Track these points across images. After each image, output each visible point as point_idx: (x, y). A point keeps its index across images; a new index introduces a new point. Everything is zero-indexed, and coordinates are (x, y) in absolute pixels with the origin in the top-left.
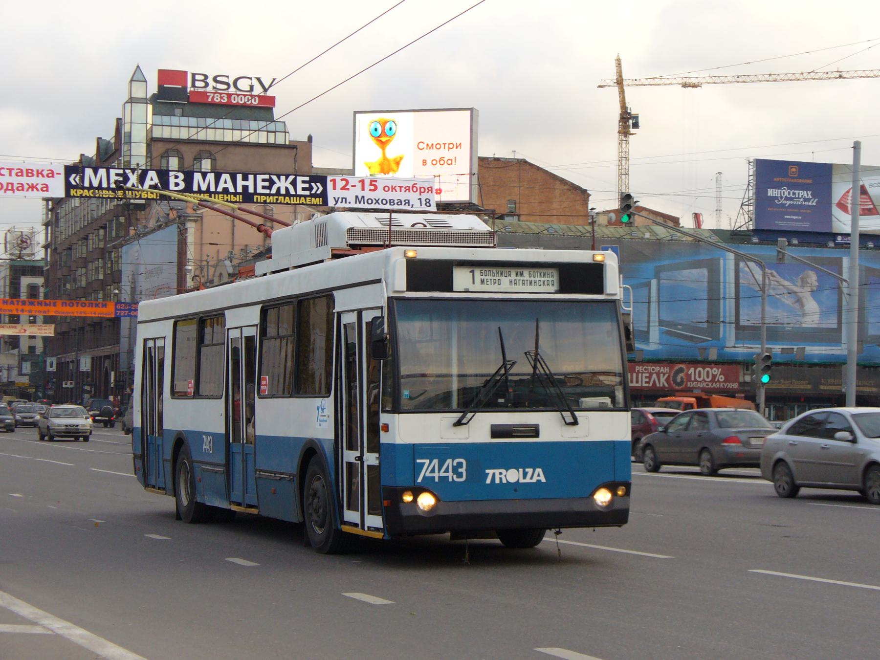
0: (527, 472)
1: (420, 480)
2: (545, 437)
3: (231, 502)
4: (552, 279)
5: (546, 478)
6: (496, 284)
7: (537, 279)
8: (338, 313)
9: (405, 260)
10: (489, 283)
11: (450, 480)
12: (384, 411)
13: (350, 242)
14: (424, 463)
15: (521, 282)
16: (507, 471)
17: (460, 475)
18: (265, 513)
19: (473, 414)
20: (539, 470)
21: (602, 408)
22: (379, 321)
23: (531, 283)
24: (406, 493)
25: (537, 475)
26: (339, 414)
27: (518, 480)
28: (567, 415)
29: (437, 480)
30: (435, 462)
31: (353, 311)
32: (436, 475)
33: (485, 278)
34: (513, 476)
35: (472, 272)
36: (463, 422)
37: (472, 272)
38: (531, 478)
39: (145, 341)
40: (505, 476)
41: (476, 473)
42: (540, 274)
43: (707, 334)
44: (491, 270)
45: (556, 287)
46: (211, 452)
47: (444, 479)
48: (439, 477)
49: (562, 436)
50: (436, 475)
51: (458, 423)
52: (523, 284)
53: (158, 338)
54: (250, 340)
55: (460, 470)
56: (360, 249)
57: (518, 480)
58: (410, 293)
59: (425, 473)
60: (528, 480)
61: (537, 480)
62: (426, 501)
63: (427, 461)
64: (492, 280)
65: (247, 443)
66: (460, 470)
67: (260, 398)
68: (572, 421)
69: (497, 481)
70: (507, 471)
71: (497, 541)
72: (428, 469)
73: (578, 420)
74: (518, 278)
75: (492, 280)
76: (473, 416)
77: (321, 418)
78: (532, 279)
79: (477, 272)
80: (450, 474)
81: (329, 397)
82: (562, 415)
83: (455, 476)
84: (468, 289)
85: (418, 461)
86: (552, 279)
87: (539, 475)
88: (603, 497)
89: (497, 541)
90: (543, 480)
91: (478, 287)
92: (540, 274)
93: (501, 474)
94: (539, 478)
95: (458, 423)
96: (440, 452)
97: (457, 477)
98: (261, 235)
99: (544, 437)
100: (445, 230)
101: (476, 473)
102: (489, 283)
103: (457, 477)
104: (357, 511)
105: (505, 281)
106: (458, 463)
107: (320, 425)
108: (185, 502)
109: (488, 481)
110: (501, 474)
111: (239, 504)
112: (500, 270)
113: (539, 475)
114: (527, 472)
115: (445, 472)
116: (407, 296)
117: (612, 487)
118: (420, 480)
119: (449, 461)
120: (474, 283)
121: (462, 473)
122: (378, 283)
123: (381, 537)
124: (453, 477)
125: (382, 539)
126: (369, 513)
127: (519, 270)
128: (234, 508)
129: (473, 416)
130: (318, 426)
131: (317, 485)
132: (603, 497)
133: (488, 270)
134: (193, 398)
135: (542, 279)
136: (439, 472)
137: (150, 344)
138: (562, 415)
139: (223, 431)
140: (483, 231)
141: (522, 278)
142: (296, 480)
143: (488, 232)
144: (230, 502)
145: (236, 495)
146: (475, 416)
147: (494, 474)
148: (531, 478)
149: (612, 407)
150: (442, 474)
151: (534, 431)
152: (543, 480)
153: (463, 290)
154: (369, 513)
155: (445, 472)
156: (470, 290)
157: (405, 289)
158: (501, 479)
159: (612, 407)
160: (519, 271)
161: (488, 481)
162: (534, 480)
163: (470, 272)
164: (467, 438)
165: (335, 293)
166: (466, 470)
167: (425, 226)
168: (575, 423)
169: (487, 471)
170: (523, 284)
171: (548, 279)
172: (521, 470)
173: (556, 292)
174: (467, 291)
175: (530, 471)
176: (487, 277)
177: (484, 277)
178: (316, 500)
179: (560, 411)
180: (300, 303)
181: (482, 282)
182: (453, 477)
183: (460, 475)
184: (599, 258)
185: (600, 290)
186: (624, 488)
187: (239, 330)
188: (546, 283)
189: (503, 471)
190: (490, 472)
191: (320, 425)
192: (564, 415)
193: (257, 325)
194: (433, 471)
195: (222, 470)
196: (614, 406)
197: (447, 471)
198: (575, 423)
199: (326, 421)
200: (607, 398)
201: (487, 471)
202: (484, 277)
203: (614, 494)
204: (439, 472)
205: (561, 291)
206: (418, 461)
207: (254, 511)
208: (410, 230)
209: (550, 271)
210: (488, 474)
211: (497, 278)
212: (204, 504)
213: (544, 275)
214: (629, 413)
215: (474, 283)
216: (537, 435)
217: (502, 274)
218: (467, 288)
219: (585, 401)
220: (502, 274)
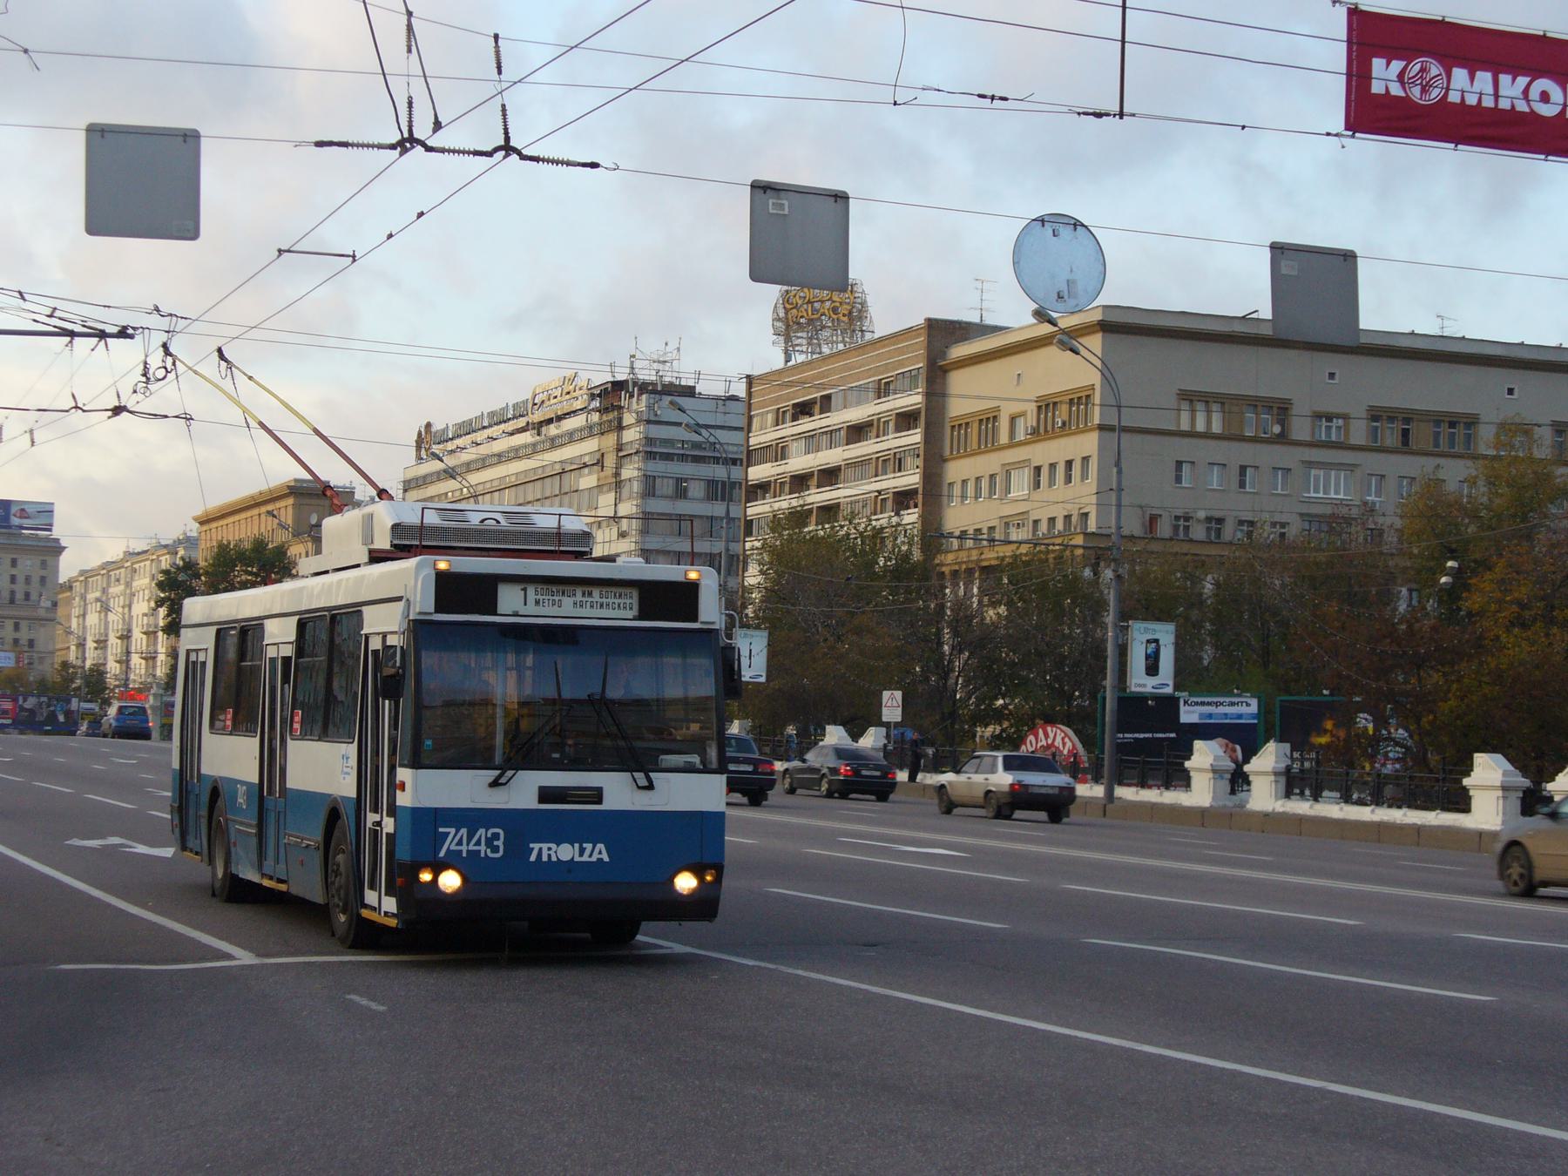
0: (585, 848)
1: (442, 854)
2: (611, 803)
3: (263, 875)
4: (631, 601)
5: (609, 857)
6: (556, 607)
7: (610, 601)
8: (366, 635)
9: (433, 572)
10: (546, 604)
11: (483, 855)
12: (402, 766)
13: (395, 542)
14: (449, 833)
15: (588, 603)
16: (558, 846)
17: (495, 849)
18: (295, 891)
19: (513, 772)
20: (600, 846)
21: (689, 769)
22: (392, 651)
23: (602, 606)
24: (423, 870)
25: (599, 852)
26: (363, 766)
27: (573, 858)
28: (640, 776)
29: (464, 855)
30: (464, 831)
31: (379, 634)
32: (464, 848)
33: (541, 598)
34: (566, 852)
35: (525, 590)
36: (500, 782)
37: (525, 590)
38: (590, 856)
39: (188, 652)
40: (556, 852)
41: (518, 848)
42: (615, 595)
43: (750, 687)
44: (550, 587)
45: (635, 612)
46: (244, 807)
47: (474, 854)
48: (468, 851)
49: (633, 804)
50: (464, 848)
51: (495, 784)
52: (592, 607)
53: (200, 650)
54: (287, 660)
55: (496, 843)
56: (409, 551)
57: (573, 858)
58: (440, 615)
59: (449, 844)
60: (585, 858)
61: (598, 859)
62: (450, 881)
63: (453, 831)
64: (551, 601)
65: (279, 797)
66: (496, 843)
67: (292, 739)
68: (647, 784)
69: (545, 858)
70: (558, 846)
71: (588, 935)
72: (454, 840)
73: (654, 783)
74: (584, 599)
75: (551, 601)
76: (514, 775)
77: (345, 770)
78: (604, 600)
79: (531, 590)
80: (483, 848)
81: (352, 743)
82: (633, 776)
83: (489, 850)
84: (517, 612)
85: (441, 830)
86: (631, 601)
87: (600, 853)
88: (685, 882)
89: (588, 935)
90: (606, 858)
91: (531, 609)
92: (615, 595)
93: (549, 849)
94: (600, 856)
95: (495, 784)
96: (471, 819)
97: (492, 852)
98: (1440, 319)
99: (608, 805)
100: (527, 529)
101: (518, 848)
102: (546, 604)
103: (492, 852)
104: (376, 891)
105: (567, 602)
106: (493, 834)
107: (344, 778)
108: (220, 874)
109: (533, 858)
110: (549, 849)
111: (271, 878)
112: (561, 588)
113: (600, 853)
114: (585, 848)
115: (475, 845)
116: (436, 619)
117: (698, 871)
118: (442, 854)
119: (482, 831)
120: (525, 604)
121: (498, 847)
122: (398, 601)
123: (394, 925)
124: (486, 851)
125: (397, 928)
126: (386, 895)
127: (587, 589)
128: (266, 883)
129: (514, 775)
130: (342, 780)
131: (340, 858)
132: (685, 882)
133: (545, 587)
134: (231, 734)
135: (617, 601)
136: (468, 845)
137: (193, 657)
138: (633, 776)
139: (256, 781)
140: (573, 530)
141: (590, 599)
142: (322, 847)
143: (581, 532)
144: (262, 874)
145: (269, 865)
146: (516, 776)
147: (541, 849)
148: (590, 856)
149: (702, 767)
150: (472, 847)
151: (596, 795)
152: (606, 858)
153: (511, 613)
154: (386, 895)
155: (475, 845)
156: (520, 613)
157: (433, 611)
158: (549, 856)
159: (702, 767)
160: (587, 590)
161: (533, 858)
162: (594, 859)
163: (522, 590)
164: (507, 803)
165: (364, 609)
166: (504, 843)
167: (498, 522)
168: (650, 787)
169: (531, 845)
170: (592, 607)
171: (625, 601)
172: (577, 845)
173: (634, 619)
174: (516, 615)
175: (588, 846)
176: (544, 597)
177: (539, 597)
178: (338, 879)
179: (631, 770)
180: (333, 617)
181: (537, 602)
182: (486, 851)
183: (495, 849)
184: (693, 575)
185: (694, 617)
186: (713, 871)
187: (276, 646)
188: (622, 605)
189: (553, 846)
190: (536, 846)
191: (344, 778)
192: (636, 777)
193: (292, 643)
194: (460, 843)
195: (254, 831)
196: (704, 765)
197: (478, 843)
198: (650, 787)
199: (349, 774)
200: (696, 756)
201: (531, 845)
202: (539, 597)
203: (701, 878)
204: (468, 845)
205: (640, 617)
206: (441, 830)
207: (283, 887)
208: (495, 528)
209: (628, 591)
210: (533, 849)
211: (557, 598)
212: (238, 876)
213: (620, 596)
214: (724, 777)
215: (525, 604)
216: (600, 802)
217: (563, 593)
218: (516, 610)
219: (665, 759)
220: (563, 593)
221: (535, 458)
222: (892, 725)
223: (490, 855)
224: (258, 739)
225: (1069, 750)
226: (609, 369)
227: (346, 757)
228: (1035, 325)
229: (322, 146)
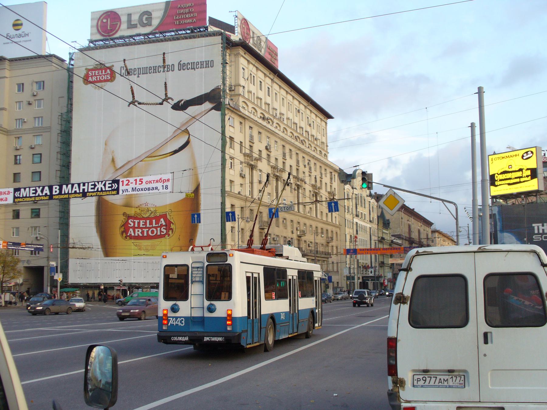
17: (182, 323)
29: (175, 325)
50: (174, 323)
55: (182, 322)
66: (182, 322)
80: (179, 323)
119: (179, 319)
150: (176, 323)
183: (182, 323)
194: (174, 322)
197: (178, 322)
221: (35, 55)
222: (354, 281)
223: (181, 325)
224: (288, 300)
225: (103, 385)
226: (346, 197)
227: (313, 300)
228: (538, 180)
229: (464, 370)
